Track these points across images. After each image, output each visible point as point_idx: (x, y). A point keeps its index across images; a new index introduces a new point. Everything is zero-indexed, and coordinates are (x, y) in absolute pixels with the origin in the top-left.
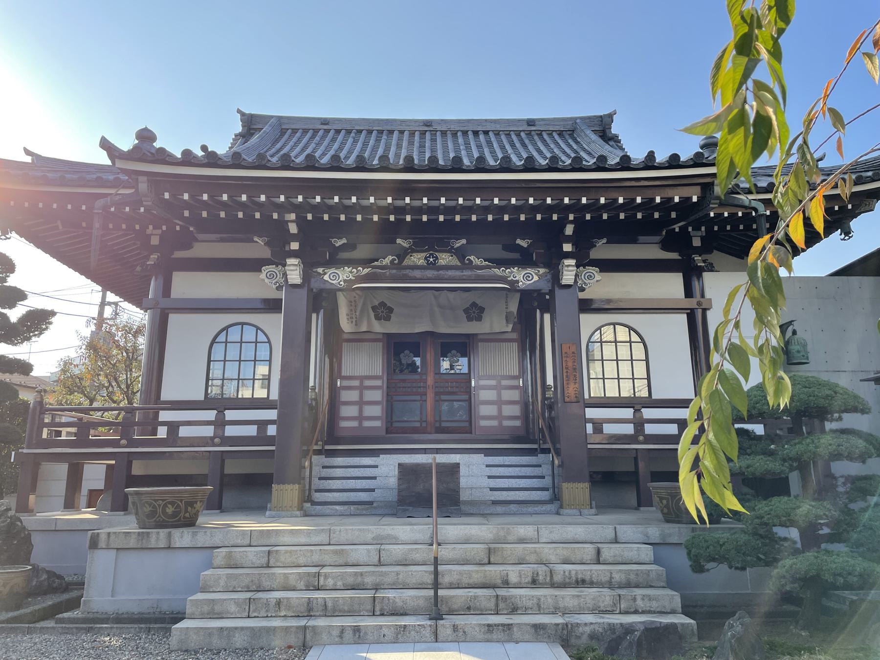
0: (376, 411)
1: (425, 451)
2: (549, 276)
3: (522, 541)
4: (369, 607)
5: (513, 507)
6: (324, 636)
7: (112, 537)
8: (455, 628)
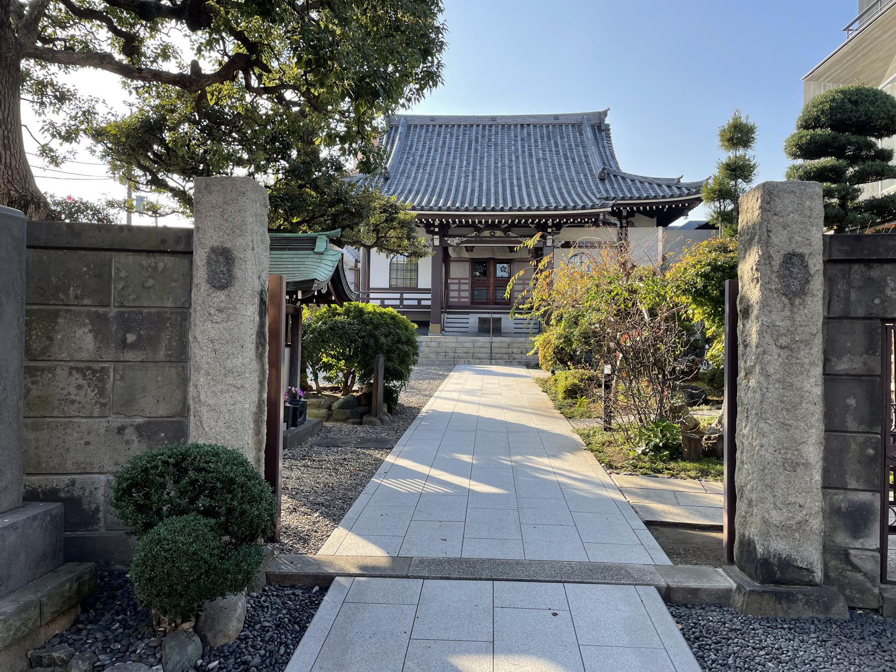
0: (467, 294)
1: (488, 313)
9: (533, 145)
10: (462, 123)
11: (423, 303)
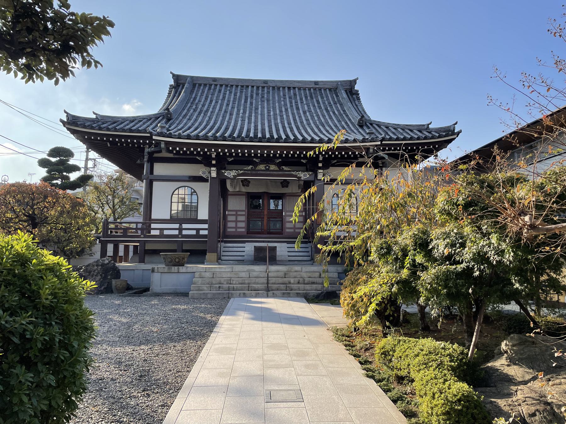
0: (243, 225)
2: (314, 175)
3: (296, 271)
4: (247, 288)
5: (296, 262)
6: (235, 295)
7: (159, 269)
8: (273, 293)
9: (299, 102)
10: (240, 84)
11: (202, 232)
